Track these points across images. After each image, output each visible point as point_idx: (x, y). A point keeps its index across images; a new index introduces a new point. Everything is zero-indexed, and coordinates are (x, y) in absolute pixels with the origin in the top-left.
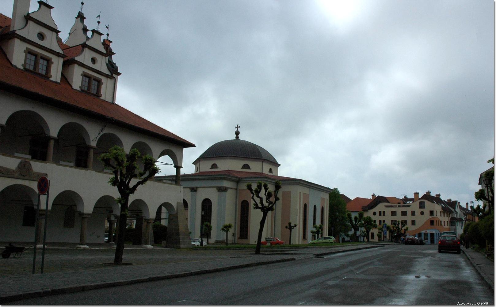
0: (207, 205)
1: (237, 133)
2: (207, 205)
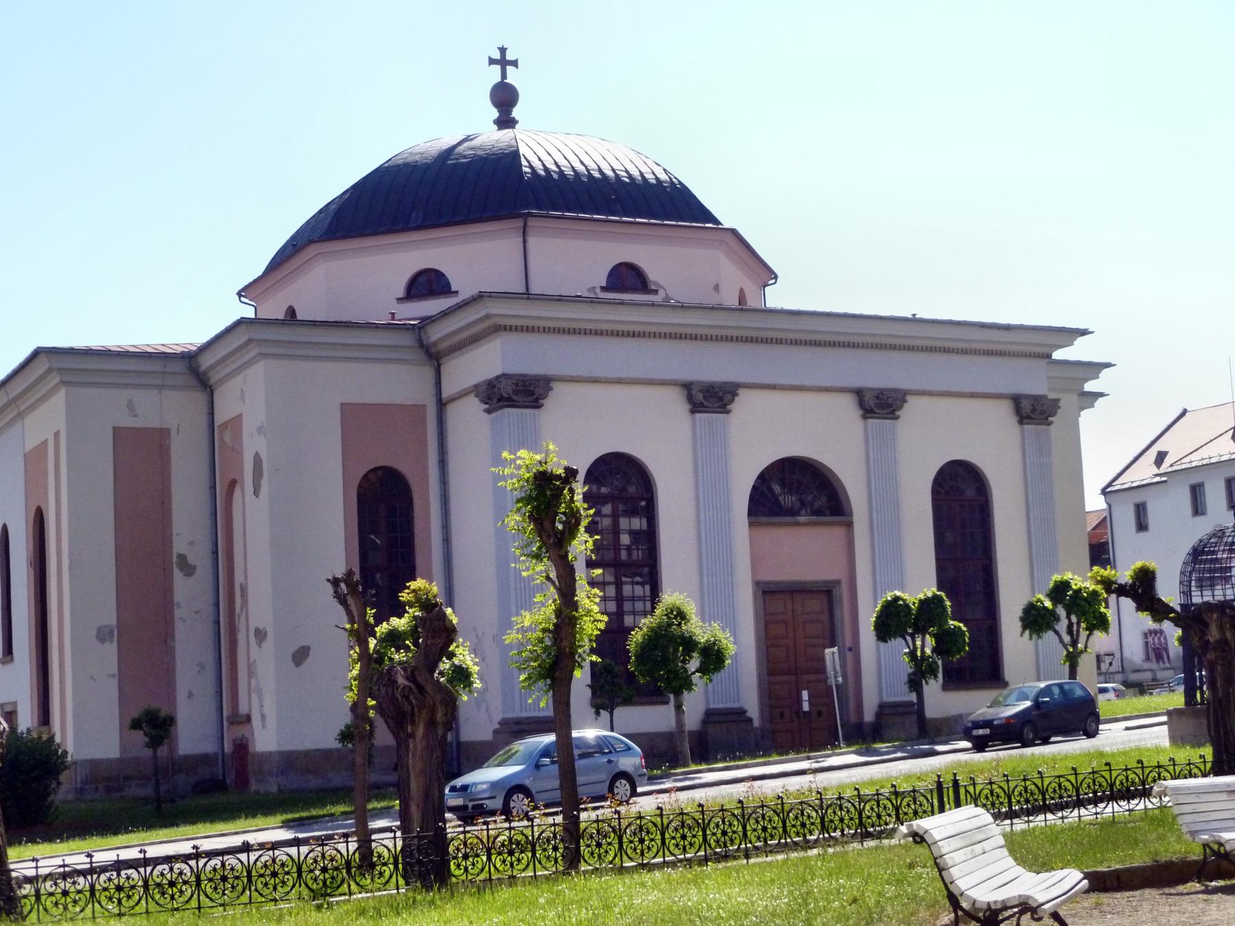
0: (961, 498)
1: (504, 98)
2: (961, 498)
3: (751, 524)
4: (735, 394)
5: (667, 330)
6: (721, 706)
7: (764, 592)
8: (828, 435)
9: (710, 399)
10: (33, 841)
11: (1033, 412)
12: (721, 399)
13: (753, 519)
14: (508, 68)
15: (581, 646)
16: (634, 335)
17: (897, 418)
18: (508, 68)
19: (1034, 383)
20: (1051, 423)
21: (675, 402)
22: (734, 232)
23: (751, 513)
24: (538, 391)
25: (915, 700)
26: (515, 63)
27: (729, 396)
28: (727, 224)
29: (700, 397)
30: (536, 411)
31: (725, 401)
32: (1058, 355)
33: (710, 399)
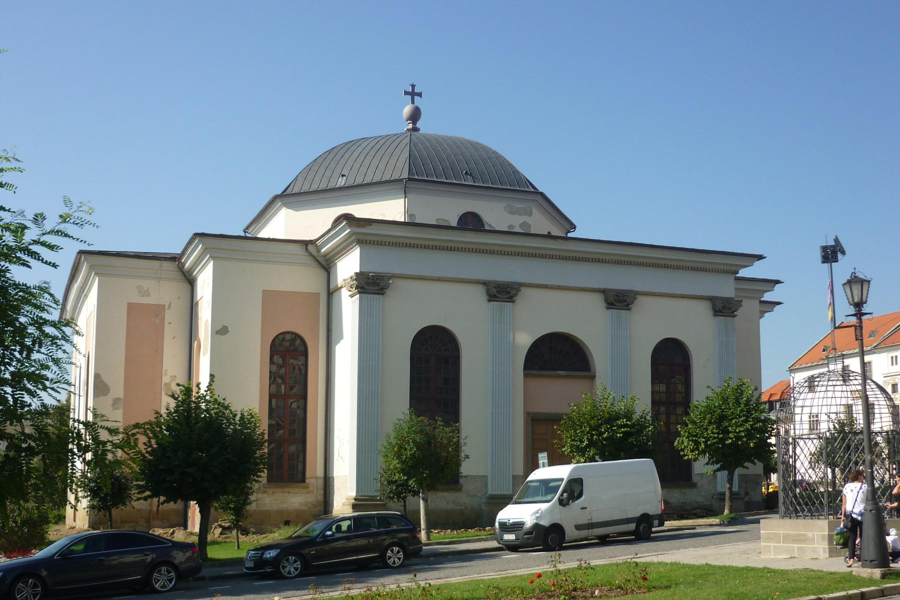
0: (671, 359)
3: (525, 375)
4: (518, 290)
5: (648, 261)
6: (499, 493)
7: (532, 420)
8: (585, 320)
9: (502, 293)
10: (289, 590)
11: (724, 308)
12: (509, 293)
13: (527, 372)
14: (416, 97)
15: (11, 424)
16: (451, 249)
17: (734, 316)
18: (416, 97)
19: (725, 289)
20: (736, 316)
21: (478, 294)
22: (542, 194)
23: (527, 367)
24: (382, 284)
25: (40, 457)
26: (406, 93)
27: (514, 291)
28: (540, 190)
29: (494, 291)
30: (381, 296)
31: (512, 294)
32: (743, 273)
33: (618, 301)
